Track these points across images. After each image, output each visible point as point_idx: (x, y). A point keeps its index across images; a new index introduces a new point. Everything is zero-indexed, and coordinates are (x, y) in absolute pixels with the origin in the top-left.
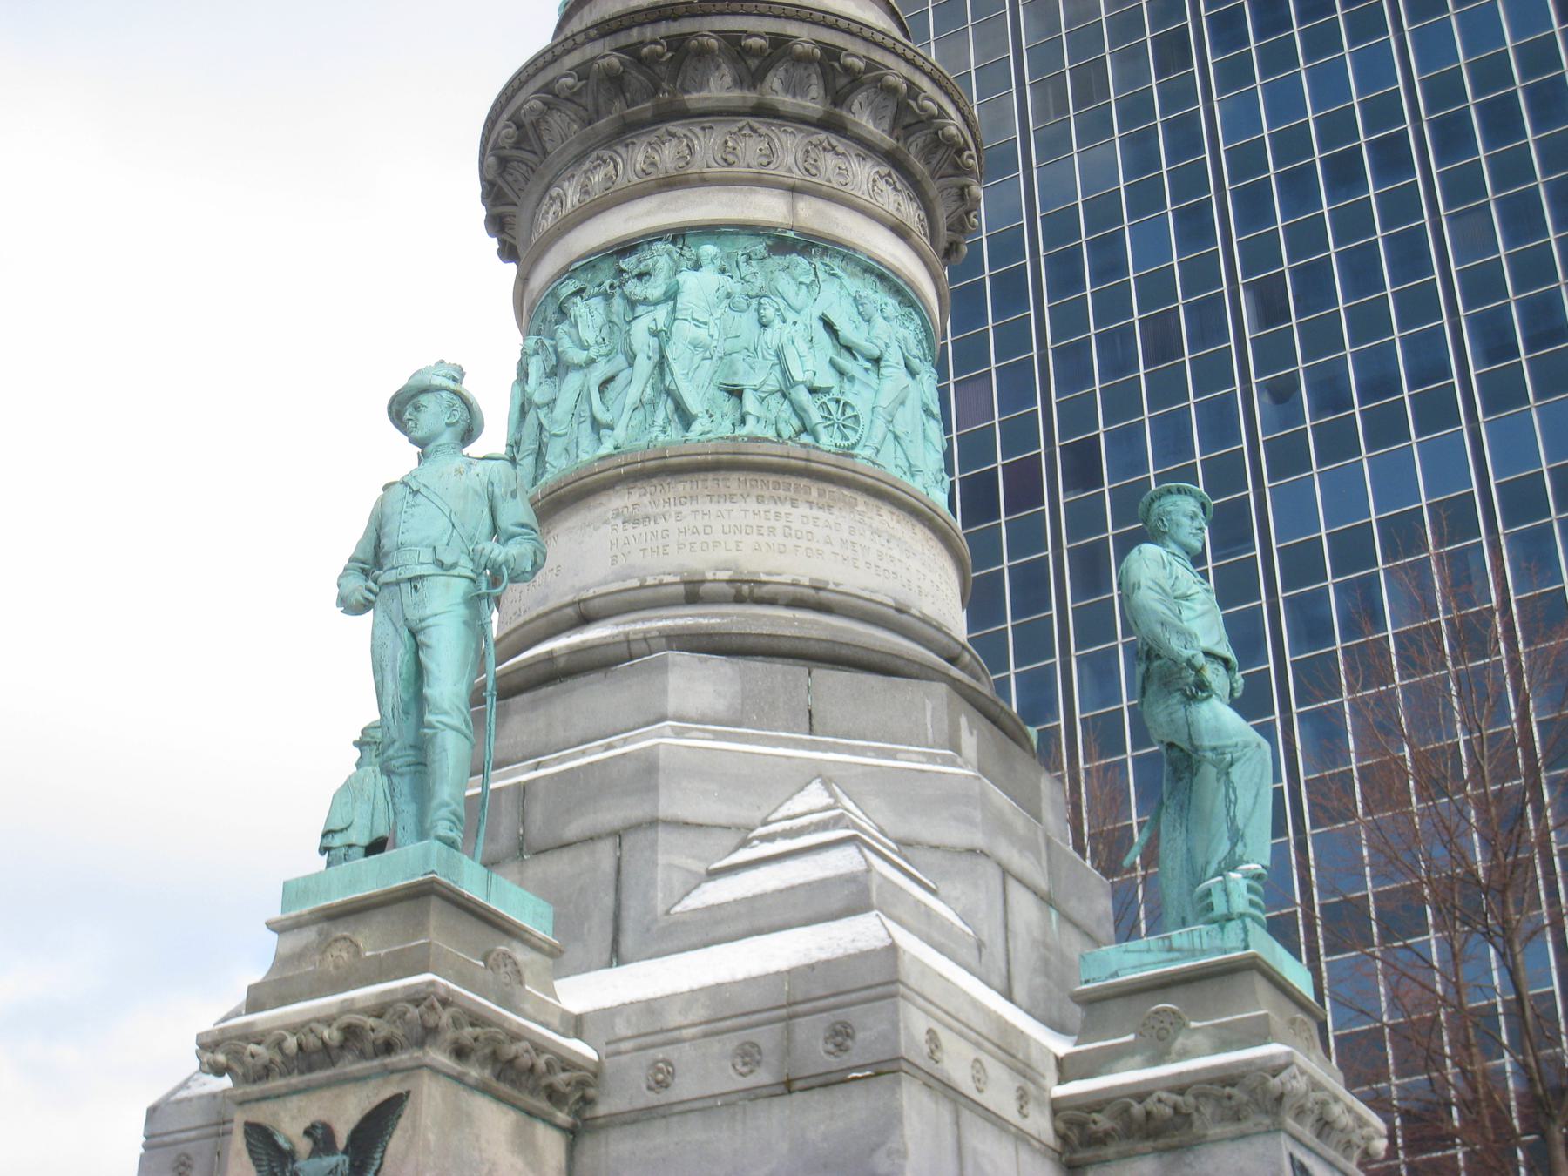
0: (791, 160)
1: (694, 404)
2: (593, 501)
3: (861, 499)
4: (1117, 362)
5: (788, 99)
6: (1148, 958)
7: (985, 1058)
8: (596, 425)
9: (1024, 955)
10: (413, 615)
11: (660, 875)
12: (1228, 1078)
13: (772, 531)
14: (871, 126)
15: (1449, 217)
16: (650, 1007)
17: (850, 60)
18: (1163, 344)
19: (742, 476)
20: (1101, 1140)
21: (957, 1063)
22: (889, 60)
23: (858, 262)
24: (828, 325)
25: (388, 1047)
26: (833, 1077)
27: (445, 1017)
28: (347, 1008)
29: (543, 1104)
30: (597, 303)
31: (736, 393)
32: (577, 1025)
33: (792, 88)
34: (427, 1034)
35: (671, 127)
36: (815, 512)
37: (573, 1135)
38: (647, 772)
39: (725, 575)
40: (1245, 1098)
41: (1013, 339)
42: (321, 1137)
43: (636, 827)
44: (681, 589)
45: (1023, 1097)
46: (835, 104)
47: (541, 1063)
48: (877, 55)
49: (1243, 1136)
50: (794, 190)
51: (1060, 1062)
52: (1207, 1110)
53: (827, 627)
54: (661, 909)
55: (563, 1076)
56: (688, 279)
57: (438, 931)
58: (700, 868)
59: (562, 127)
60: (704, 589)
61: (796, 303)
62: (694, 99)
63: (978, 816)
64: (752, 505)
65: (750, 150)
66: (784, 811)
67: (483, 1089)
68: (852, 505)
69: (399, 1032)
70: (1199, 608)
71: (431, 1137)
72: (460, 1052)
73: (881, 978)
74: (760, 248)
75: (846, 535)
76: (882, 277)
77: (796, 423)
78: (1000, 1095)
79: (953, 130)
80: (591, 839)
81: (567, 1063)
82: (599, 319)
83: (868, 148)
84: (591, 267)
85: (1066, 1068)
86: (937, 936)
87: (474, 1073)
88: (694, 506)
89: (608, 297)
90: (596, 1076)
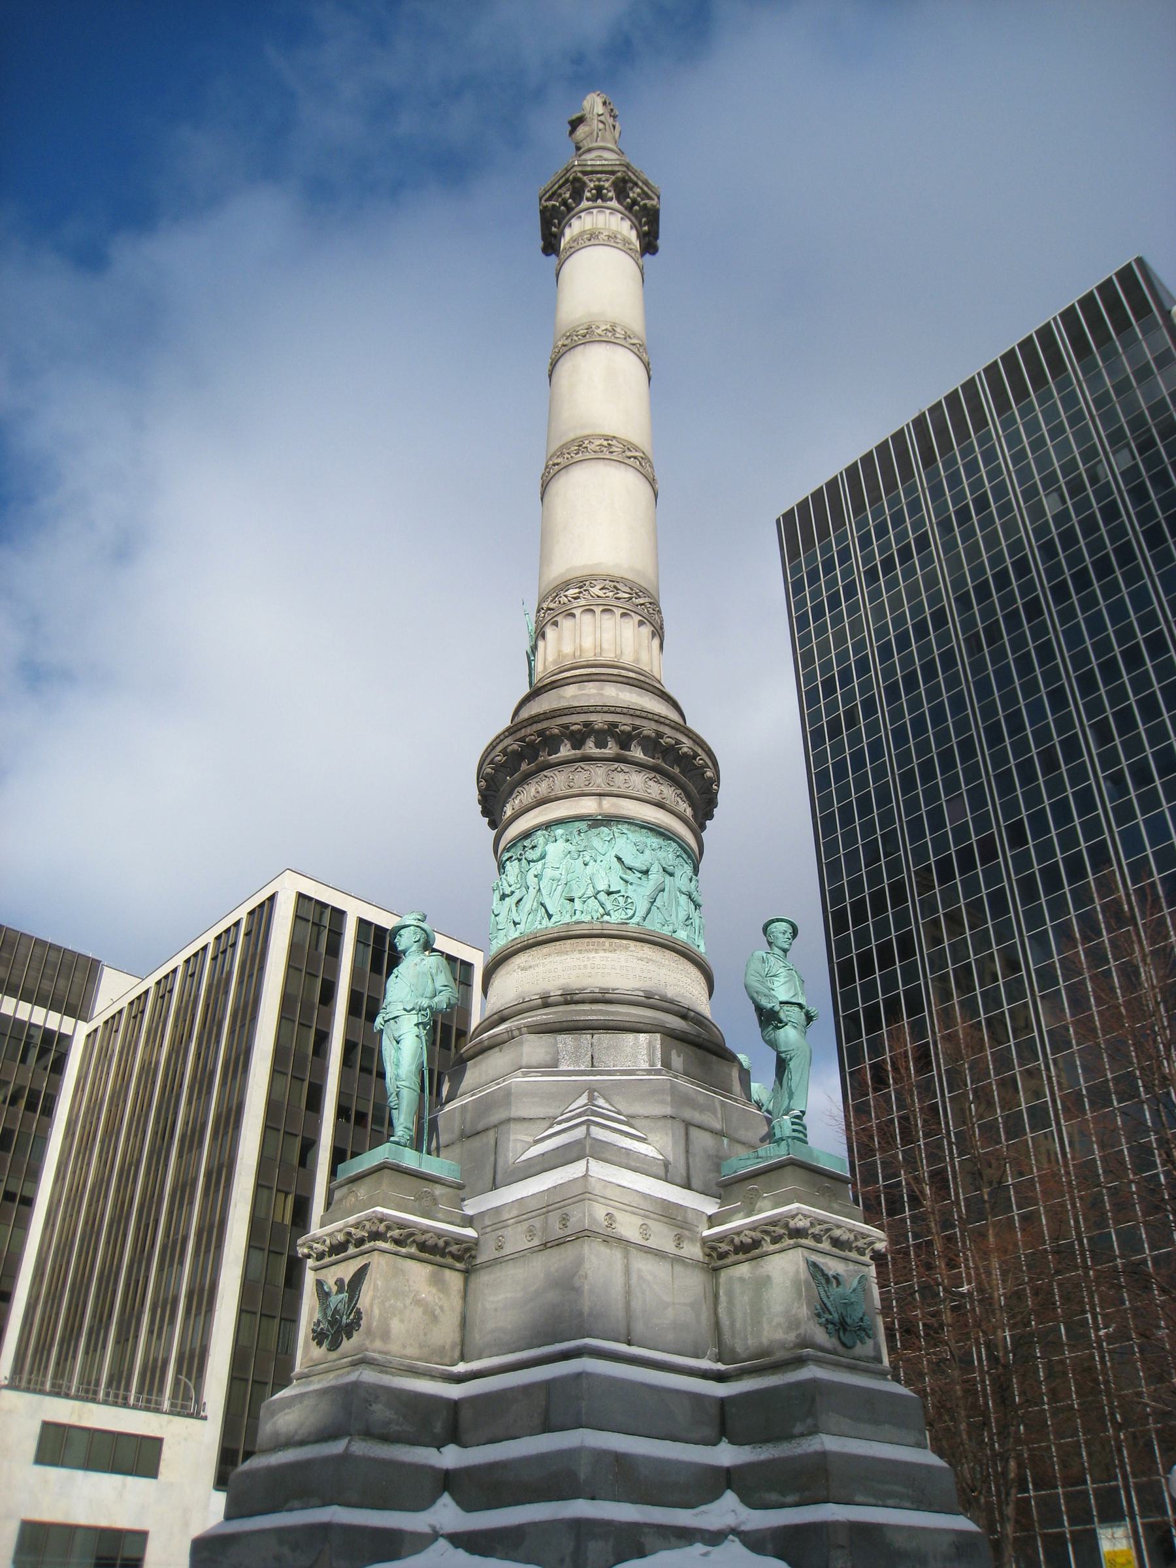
0: (599, 781)
4: (1028, 775)
5: (598, 750)
7: (649, 1222)
8: (515, 924)
9: (698, 1163)
10: (396, 1035)
11: (511, 1145)
17: (623, 728)
18: (1050, 764)
20: (722, 1256)
21: (629, 1227)
22: (645, 723)
23: (637, 825)
24: (619, 859)
25: (360, 1242)
26: (562, 1241)
29: (449, 1260)
31: (572, 900)
32: (469, 1221)
34: (376, 1236)
35: (545, 773)
36: (608, 954)
37: (467, 1273)
39: (559, 993)
40: (782, 1231)
42: (340, 1282)
45: (679, 1240)
47: (441, 1243)
48: (638, 722)
51: (710, 1217)
54: (511, 1162)
56: (551, 848)
58: (530, 1139)
60: (551, 1000)
63: (669, 1099)
64: (576, 955)
67: (411, 1257)
71: (379, 1283)
73: (582, 1192)
74: (583, 825)
76: (651, 829)
77: (601, 911)
79: (685, 750)
80: (486, 1130)
81: (459, 1240)
82: (517, 871)
83: (641, 766)
85: (712, 1221)
86: (633, 1164)
89: (520, 860)
90: (476, 1245)
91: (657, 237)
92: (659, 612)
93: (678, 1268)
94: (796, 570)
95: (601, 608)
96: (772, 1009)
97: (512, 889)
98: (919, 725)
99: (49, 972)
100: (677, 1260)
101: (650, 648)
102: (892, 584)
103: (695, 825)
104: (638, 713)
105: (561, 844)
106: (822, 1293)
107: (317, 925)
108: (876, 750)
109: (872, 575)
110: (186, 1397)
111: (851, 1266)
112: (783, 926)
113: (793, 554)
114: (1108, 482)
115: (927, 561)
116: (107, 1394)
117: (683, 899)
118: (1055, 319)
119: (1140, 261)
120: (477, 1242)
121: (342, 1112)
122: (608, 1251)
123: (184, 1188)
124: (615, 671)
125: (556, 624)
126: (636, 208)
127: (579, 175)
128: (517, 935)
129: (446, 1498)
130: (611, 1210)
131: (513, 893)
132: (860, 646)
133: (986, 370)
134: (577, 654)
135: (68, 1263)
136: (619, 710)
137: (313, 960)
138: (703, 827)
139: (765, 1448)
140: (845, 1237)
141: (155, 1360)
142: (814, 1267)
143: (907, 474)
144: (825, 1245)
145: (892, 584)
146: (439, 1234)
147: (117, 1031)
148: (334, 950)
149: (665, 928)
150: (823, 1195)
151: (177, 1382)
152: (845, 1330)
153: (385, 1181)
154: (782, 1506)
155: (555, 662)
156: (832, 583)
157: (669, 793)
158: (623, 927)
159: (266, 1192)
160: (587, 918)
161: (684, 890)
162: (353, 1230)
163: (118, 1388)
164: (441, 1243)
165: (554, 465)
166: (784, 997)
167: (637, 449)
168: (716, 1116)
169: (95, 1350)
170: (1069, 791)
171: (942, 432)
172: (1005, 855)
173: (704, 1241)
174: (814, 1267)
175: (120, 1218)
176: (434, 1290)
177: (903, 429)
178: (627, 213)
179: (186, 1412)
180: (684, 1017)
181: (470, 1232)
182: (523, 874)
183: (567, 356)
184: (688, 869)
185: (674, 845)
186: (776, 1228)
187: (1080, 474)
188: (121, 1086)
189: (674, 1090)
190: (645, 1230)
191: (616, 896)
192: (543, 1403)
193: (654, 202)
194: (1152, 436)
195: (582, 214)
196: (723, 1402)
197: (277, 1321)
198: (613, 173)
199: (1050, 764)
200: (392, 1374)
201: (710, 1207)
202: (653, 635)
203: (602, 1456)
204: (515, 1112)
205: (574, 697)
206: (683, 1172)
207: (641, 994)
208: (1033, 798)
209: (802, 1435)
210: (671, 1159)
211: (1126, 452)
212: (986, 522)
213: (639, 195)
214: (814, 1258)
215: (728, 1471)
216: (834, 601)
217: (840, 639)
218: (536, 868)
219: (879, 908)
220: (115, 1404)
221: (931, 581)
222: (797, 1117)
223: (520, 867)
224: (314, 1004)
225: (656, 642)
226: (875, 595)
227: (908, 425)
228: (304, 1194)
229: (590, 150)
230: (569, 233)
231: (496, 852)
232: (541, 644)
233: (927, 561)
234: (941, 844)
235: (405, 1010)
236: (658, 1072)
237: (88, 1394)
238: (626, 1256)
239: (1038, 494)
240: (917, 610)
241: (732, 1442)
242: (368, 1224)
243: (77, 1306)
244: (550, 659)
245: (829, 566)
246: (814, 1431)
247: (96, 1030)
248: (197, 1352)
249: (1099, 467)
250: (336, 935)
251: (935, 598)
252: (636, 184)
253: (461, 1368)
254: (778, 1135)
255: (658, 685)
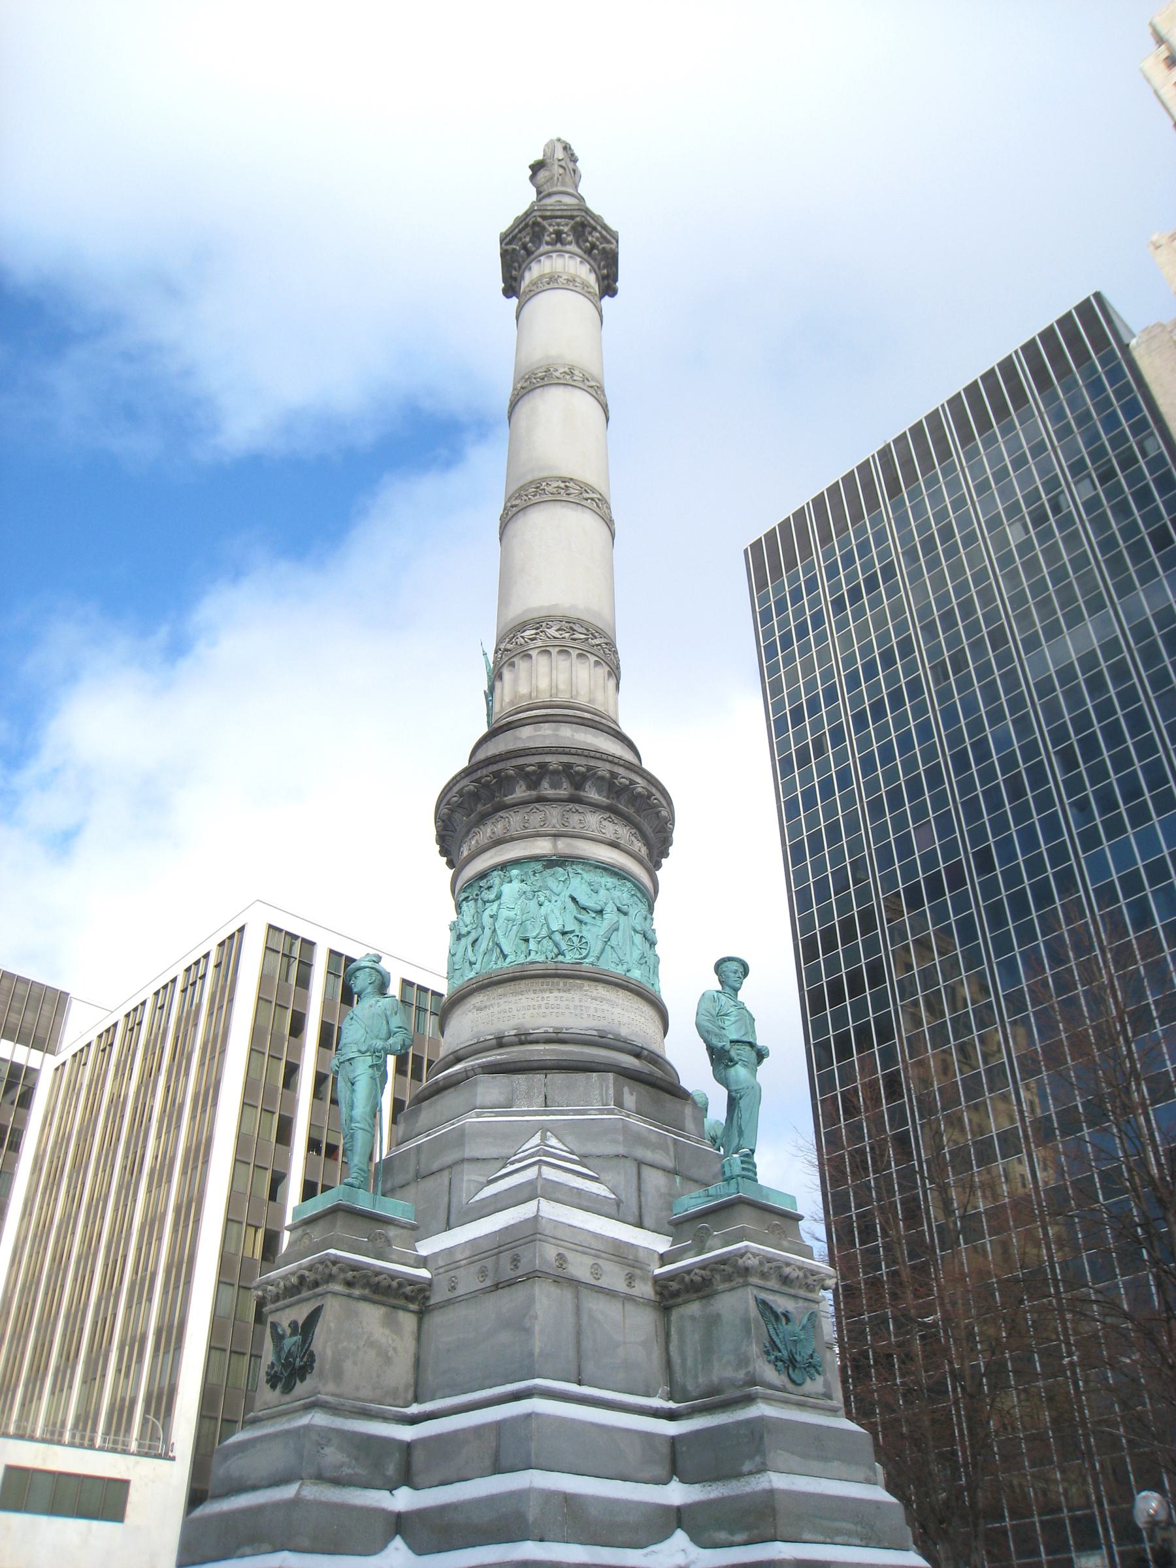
0: (554, 821)
1: (506, 950)
2: (465, 1001)
3: (586, 984)
6: (699, 1201)
7: (600, 1262)
8: (471, 964)
11: (465, 1185)
12: (723, 1261)
13: (540, 1006)
14: (596, 797)
15: (1156, 698)
16: (450, 1251)
18: (1016, 791)
19: (526, 981)
20: (676, 1294)
21: (580, 1267)
22: (599, 764)
24: (573, 899)
25: (316, 1284)
27: (335, 1270)
28: (300, 1268)
29: (402, 1302)
30: (472, 903)
32: (423, 1262)
33: (554, 786)
34: (330, 1278)
35: (501, 814)
36: (561, 994)
37: (421, 1314)
38: (460, 1137)
41: (940, 801)
42: (293, 1325)
43: (456, 1163)
44: (494, 1042)
45: (630, 1279)
46: (577, 789)
48: (592, 763)
49: (733, 1289)
50: (556, 836)
51: (661, 1256)
52: (718, 1277)
53: (564, 1052)
54: (464, 1201)
55: (410, 1288)
56: (506, 888)
57: (340, 1229)
58: (484, 1180)
59: (461, 819)
61: (557, 891)
62: (509, 799)
63: (621, 1138)
65: (535, 819)
66: (524, 1148)
67: (364, 1298)
68: (581, 987)
69: (319, 1277)
70: (733, 1019)
71: (332, 1325)
72: (349, 1284)
74: (538, 866)
75: (577, 1003)
76: (605, 869)
77: (556, 951)
78: (614, 1278)
79: (640, 790)
81: (412, 1281)
82: (473, 911)
83: (596, 807)
84: (470, 886)
85: (664, 1259)
86: (585, 1203)
87: (357, 1292)
88: (505, 999)
89: (476, 900)
91: (616, 280)
92: (616, 652)
93: (629, 1307)
94: (764, 599)
95: (558, 649)
96: (723, 1047)
97: (469, 929)
98: (887, 753)
99: (16, 1005)
100: (628, 1298)
101: (605, 688)
102: (859, 613)
103: (650, 865)
104: (592, 754)
105: (516, 885)
106: (772, 1331)
107: (288, 956)
108: (845, 778)
109: (838, 605)
110: (154, 1437)
111: (801, 1303)
112: (734, 966)
113: (762, 585)
114: (1070, 512)
115: (893, 591)
116: (73, 1436)
117: (638, 938)
118: (1016, 352)
119: (1098, 296)
120: (430, 1283)
121: (313, 1145)
122: (559, 1291)
123: (153, 1222)
124: (570, 712)
125: (512, 665)
126: (595, 251)
127: (539, 219)
128: (472, 974)
129: (398, 1542)
130: (561, 1250)
131: (469, 933)
132: (827, 675)
133: (950, 402)
134: (534, 695)
135: (34, 1301)
136: (573, 751)
137: (282, 991)
138: (658, 865)
139: (714, 1486)
140: (794, 1274)
141: (123, 1399)
142: (764, 1305)
143: (873, 504)
144: (773, 1283)
145: (859, 613)
146: (393, 1276)
147: (85, 1064)
148: (304, 981)
149: (620, 967)
150: (773, 1232)
151: (145, 1421)
152: (794, 1368)
153: (339, 1223)
154: (731, 1545)
155: (512, 703)
156: (799, 612)
157: (624, 833)
158: (577, 967)
159: (235, 1226)
160: (542, 958)
161: (638, 928)
162: (307, 1273)
163: (85, 1429)
164: (395, 1284)
165: (512, 506)
166: (734, 1037)
167: (594, 491)
168: (668, 1154)
169: (62, 1390)
170: (1036, 817)
171: (907, 463)
172: (973, 881)
173: (656, 1280)
174: (764, 1305)
175: (88, 1255)
176: (387, 1332)
177: (868, 460)
178: (585, 256)
179: (153, 1452)
180: (638, 1056)
181: (424, 1273)
182: (478, 914)
183: (526, 398)
184: (643, 908)
185: (629, 884)
186: (725, 1267)
187: (1043, 504)
188: (90, 1119)
189: (626, 1128)
190: (596, 1271)
191: (571, 936)
192: (494, 1445)
193: (613, 246)
194: (1113, 467)
195: (542, 258)
196: (674, 1441)
197: (247, 1357)
198: (572, 217)
199: (1016, 791)
200: (345, 1417)
201: (662, 1244)
202: (610, 674)
203: (549, 1496)
204: (469, 1153)
205: (529, 738)
206: (635, 1210)
207: (595, 1033)
208: (1000, 825)
209: (751, 1473)
210: (623, 1198)
211: (1087, 482)
212: (951, 552)
213: (597, 239)
214: (763, 1295)
215: (679, 1510)
216: (802, 631)
217: (808, 668)
218: (492, 908)
219: (849, 935)
220: (81, 1446)
221: (897, 610)
222: (747, 1155)
223: (476, 908)
224: (284, 1036)
225: (611, 683)
226: (842, 624)
227: (873, 456)
228: (276, 1229)
229: (550, 195)
230: (529, 277)
231: (453, 892)
232: (498, 685)
233: (893, 591)
234: (909, 871)
235: (359, 1051)
236: (611, 1112)
237: (53, 1437)
238: (577, 1296)
239: (1002, 524)
240: (884, 638)
241: (682, 1481)
242: (321, 1268)
243: (43, 1345)
244: (507, 699)
245: (796, 596)
246: (762, 1469)
247: (64, 1064)
248: (155, 1394)
249: (1061, 497)
250: (306, 966)
251: (901, 627)
252: (595, 229)
253: (415, 1409)
254: (728, 1174)
255: (613, 725)
